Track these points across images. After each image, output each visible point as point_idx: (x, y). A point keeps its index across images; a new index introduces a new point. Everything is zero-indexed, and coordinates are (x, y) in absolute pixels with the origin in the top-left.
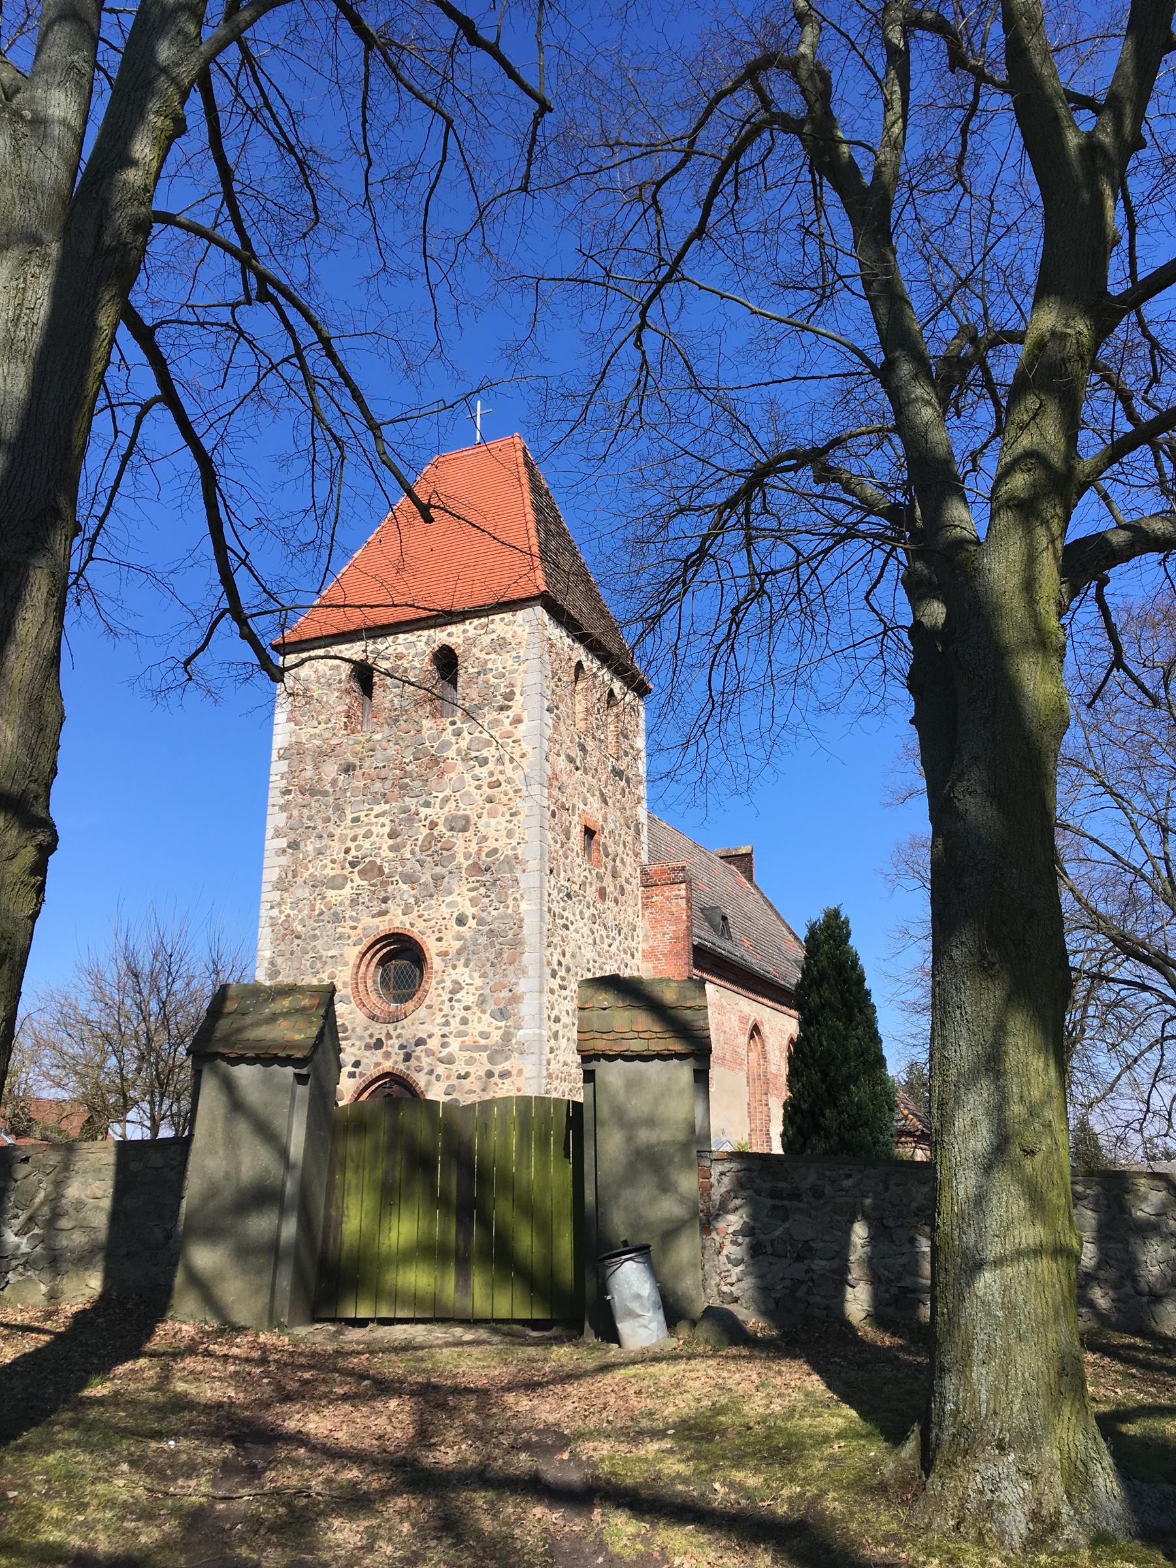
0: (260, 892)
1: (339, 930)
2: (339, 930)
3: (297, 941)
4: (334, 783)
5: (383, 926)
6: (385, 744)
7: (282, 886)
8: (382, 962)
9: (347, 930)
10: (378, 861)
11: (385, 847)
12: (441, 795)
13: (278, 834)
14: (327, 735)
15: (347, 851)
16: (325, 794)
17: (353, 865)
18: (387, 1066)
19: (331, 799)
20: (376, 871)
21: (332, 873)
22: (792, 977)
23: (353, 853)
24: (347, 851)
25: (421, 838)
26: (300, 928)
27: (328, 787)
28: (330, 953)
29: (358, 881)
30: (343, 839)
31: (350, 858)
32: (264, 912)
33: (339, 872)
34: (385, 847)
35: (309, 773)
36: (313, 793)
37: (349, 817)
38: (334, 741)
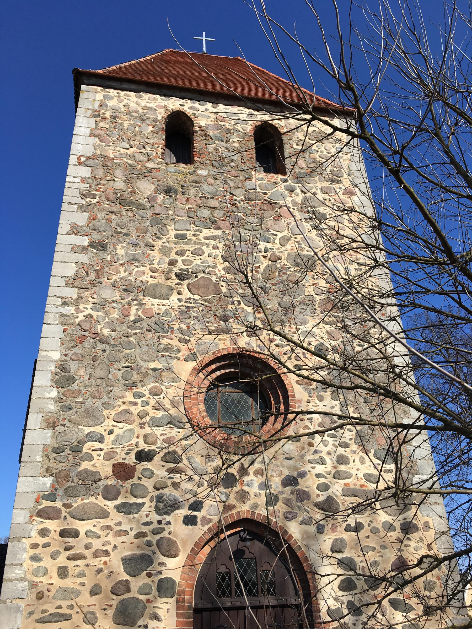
0: (47, 285)
1: (164, 341)
2: (164, 341)
3: (100, 346)
4: (151, 199)
5: (224, 345)
6: (211, 181)
7: (85, 281)
8: (214, 385)
9: (175, 343)
10: (214, 278)
11: (220, 267)
12: (280, 235)
13: (75, 230)
14: (141, 157)
15: (172, 263)
16: (141, 207)
17: (181, 276)
18: (243, 509)
19: (149, 213)
20: (212, 288)
21: (151, 281)
22: (200, 615)
23: (180, 265)
24: (172, 263)
25: (262, 268)
26: (106, 332)
27: (144, 202)
28: (152, 365)
29: (186, 294)
30: (165, 251)
31: (176, 270)
32: (52, 308)
33: (162, 281)
34: (220, 267)
35: (119, 184)
36: (123, 202)
37: (172, 233)
38: (150, 165)
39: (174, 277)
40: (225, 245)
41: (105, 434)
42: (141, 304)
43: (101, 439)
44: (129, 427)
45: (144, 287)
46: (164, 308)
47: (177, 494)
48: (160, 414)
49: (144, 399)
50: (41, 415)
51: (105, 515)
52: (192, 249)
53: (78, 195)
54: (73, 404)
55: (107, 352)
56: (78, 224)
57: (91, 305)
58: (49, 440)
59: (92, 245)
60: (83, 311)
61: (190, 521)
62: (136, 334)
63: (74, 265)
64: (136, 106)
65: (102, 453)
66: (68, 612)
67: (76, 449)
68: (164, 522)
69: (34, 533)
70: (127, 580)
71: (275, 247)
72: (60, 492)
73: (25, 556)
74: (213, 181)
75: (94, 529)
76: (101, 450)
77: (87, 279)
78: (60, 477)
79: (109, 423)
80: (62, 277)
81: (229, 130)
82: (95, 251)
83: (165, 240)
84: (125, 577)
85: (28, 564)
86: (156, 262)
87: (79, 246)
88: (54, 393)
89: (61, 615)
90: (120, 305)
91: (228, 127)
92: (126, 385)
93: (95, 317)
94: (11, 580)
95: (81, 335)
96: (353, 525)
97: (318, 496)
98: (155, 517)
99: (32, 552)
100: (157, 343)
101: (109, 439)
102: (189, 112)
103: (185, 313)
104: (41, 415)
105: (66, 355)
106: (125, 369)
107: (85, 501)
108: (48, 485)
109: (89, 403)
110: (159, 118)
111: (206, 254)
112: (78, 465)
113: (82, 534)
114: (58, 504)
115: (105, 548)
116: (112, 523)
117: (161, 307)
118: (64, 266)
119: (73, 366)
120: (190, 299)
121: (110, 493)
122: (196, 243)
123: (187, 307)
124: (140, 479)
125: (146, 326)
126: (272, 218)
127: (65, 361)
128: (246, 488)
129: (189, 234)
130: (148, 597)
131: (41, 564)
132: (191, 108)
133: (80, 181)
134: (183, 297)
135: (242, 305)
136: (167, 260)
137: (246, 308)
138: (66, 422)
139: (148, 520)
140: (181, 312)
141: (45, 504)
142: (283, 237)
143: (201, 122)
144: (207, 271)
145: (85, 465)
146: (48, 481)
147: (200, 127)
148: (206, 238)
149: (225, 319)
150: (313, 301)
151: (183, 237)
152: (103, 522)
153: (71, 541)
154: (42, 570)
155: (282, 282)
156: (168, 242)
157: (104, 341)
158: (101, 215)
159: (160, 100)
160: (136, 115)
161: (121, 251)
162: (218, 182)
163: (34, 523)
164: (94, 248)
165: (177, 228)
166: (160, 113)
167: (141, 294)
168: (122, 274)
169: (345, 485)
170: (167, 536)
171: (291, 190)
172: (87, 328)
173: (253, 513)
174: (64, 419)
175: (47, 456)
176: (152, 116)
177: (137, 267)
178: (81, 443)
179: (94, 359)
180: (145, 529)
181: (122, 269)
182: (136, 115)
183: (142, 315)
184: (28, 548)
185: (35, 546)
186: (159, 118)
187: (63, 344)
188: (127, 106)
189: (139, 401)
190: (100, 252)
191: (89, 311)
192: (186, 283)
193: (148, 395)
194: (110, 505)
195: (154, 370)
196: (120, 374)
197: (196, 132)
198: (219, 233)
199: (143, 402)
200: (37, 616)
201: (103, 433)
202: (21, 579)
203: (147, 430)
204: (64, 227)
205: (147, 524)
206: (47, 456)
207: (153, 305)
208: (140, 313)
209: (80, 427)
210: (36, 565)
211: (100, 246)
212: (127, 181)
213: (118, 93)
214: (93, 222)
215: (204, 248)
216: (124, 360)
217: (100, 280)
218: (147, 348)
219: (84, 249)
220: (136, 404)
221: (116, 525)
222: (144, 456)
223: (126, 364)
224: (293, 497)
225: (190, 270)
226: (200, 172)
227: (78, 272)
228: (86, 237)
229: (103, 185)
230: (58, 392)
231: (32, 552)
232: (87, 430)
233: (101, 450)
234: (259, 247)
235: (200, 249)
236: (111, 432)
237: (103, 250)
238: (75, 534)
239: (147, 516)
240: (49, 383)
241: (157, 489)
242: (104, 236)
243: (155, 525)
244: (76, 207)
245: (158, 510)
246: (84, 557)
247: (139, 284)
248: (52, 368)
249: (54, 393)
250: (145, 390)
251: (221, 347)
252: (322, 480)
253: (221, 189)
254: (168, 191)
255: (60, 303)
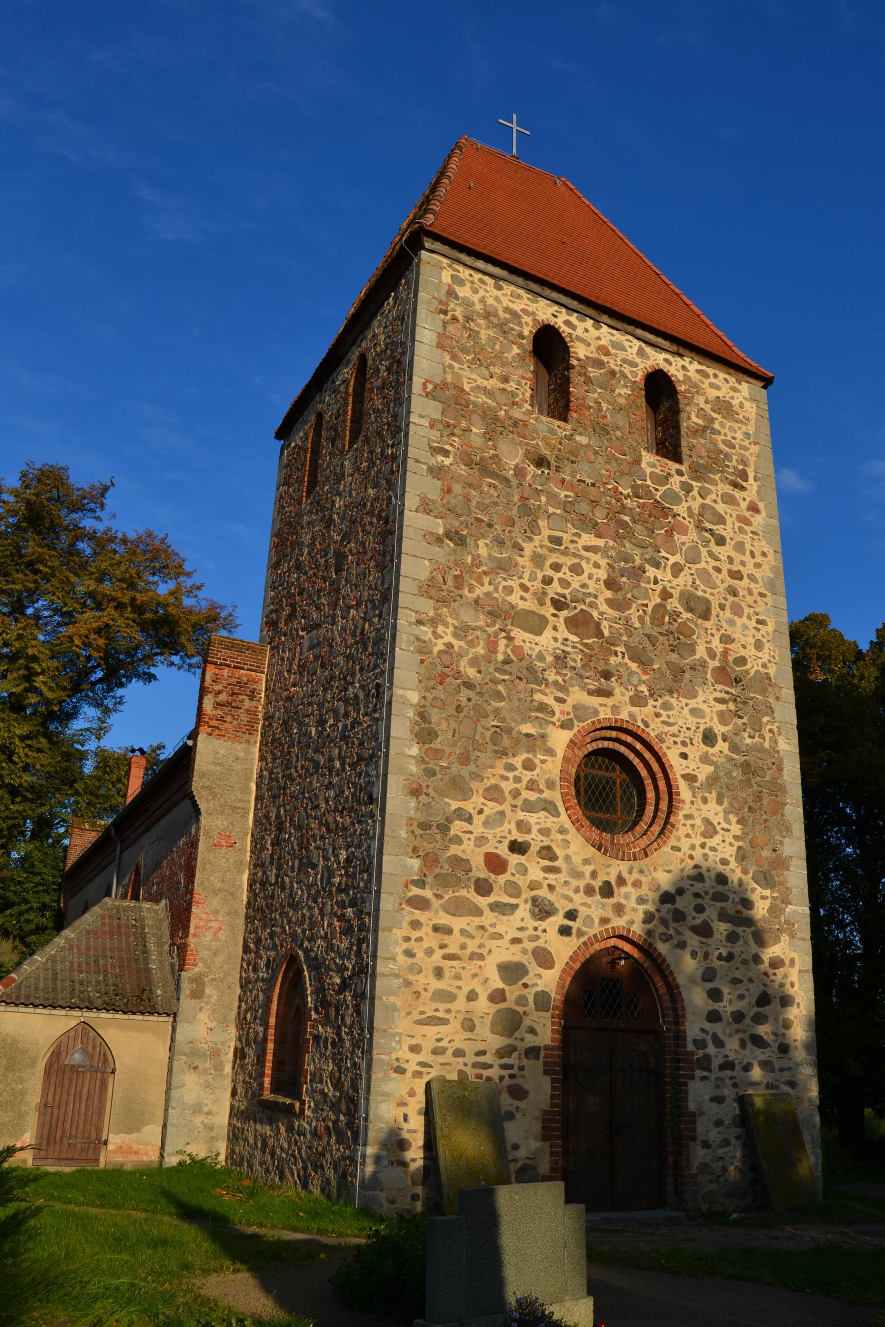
3: (465, 693)
7: (443, 590)
9: (549, 700)
10: (595, 614)
13: (426, 507)
17: (559, 605)
26: (471, 672)
37: (546, 533)
39: (549, 603)
40: (608, 564)
41: (474, 813)
42: (510, 639)
43: (469, 820)
44: (500, 808)
45: (512, 612)
46: (537, 649)
47: (551, 897)
48: (533, 796)
49: (516, 773)
50: (402, 777)
51: (478, 912)
52: (569, 563)
53: (427, 449)
54: (437, 769)
55: (473, 702)
56: (429, 496)
57: (451, 629)
58: (413, 812)
59: (447, 535)
60: (442, 637)
61: (565, 931)
62: (504, 681)
63: (427, 562)
64: (495, 303)
65: (472, 837)
66: (447, 1016)
67: (444, 828)
68: (540, 929)
69: (405, 924)
70: (503, 990)
71: (664, 575)
72: (429, 879)
73: (399, 950)
74: (592, 458)
75: (468, 928)
76: (471, 832)
77: (444, 587)
78: (430, 860)
79: (477, 800)
80: (414, 579)
81: (613, 373)
82: (452, 545)
83: (537, 543)
84: (500, 985)
85: (402, 959)
86: (526, 576)
87: (432, 533)
88: (414, 751)
89: (439, 1019)
90: (485, 636)
91: (613, 366)
92: (495, 752)
93: (456, 648)
94: (385, 975)
95: (441, 673)
96: (725, 954)
97: (694, 918)
98: (531, 923)
99: (405, 946)
100: (529, 699)
101: (478, 820)
102: (565, 330)
103: (561, 660)
104: (402, 777)
105: (425, 698)
106: (494, 729)
107: (457, 894)
108: (416, 869)
109: (455, 769)
110: (526, 333)
111: (586, 574)
112: (446, 848)
113: (456, 932)
114: (427, 893)
115: (479, 951)
116: (486, 924)
117: (533, 646)
118: (416, 563)
119: (435, 715)
120: (566, 640)
121: (483, 888)
122: (575, 555)
123: (564, 651)
124: (513, 875)
125: (515, 671)
126: (663, 532)
127: (424, 706)
128: (622, 901)
129: (566, 537)
130: (524, 1009)
131: (415, 960)
132: (567, 323)
133: (427, 424)
134: (560, 637)
135: (626, 660)
136: (540, 576)
137: (630, 663)
138: (431, 791)
139: (523, 924)
140: (557, 657)
141: (415, 891)
142: (676, 564)
143: (580, 351)
144: (588, 600)
145: (454, 850)
146: (415, 863)
147: (578, 359)
148: (587, 549)
149: (607, 675)
150: (704, 665)
151: (557, 541)
152: (477, 921)
153: (446, 939)
154: (416, 967)
155: (672, 633)
156: (541, 546)
157: (469, 685)
158: (457, 488)
159: (526, 301)
160: (495, 321)
161: (483, 551)
162: (600, 459)
163: (404, 912)
164: (451, 540)
165: (551, 526)
166: (527, 324)
167: (509, 622)
168: (487, 588)
169: (722, 908)
170: (543, 945)
171: (688, 489)
172: (448, 663)
173: (629, 930)
174: (428, 787)
175: (413, 832)
176: (516, 328)
177: (505, 579)
178: (450, 821)
179: (459, 709)
180: (519, 935)
181: (486, 580)
182: (495, 321)
183: (512, 656)
184: (400, 941)
185: (407, 939)
186: (526, 333)
187: (420, 681)
188: (482, 301)
189: (511, 775)
190: (459, 548)
191: (449, 638)
192: (564, 614)
193: (520, 769)
194: (483, 902)
195: (528, 736)
196: (488, 734)
197: (573, 367)
198: (600, 542)
199: (515, 777)
200: (416, 1016)
201: (471, 811)
202: (397, 976)
203: (521, 815)
204: (411, 501)
205: (521, 929)
206: (413, 832)
207: (524, 641)
208: (509, 650)
209: (446, 800)
210: (410, 961)
211: (460, 541)
212: (489, 436)
213: (471, 275)
214: (448, 497)
215: (584, 563)
216: (492, 717)
217: (460, 592)
218: (517, 703)
219: (439, 540)
220: (507, 779)
221: (491, 926)
222: (517, 848)
223: (494, 723)
224: (669, 917)
225: (569, 597)
226: (578, 438)
227: (432, 579)
228: (440, 521)
229: (458, 436)
230: (420, 749)
231: (405, 946)
232: (455, 805)
233: (471, 832)
234: (647, 574)
235: (579, 564)
236: (480, 812)
237: (461, 545)
238: (449, 931)
239: (522, 920)
240: (408, 735)
241: (532, 889)
242: (461, 523)
243: (531, 932)
244: (425, 467)
245: (533, 915)
246: (459, 959)
247: (507, 607)
248: (411, 714)
249: (414, 751)
250: (518, 761)
251: (601, 716)
252: (699, 901)
253: (603, 472)
254: (540, 462)
255: (413, 620)
